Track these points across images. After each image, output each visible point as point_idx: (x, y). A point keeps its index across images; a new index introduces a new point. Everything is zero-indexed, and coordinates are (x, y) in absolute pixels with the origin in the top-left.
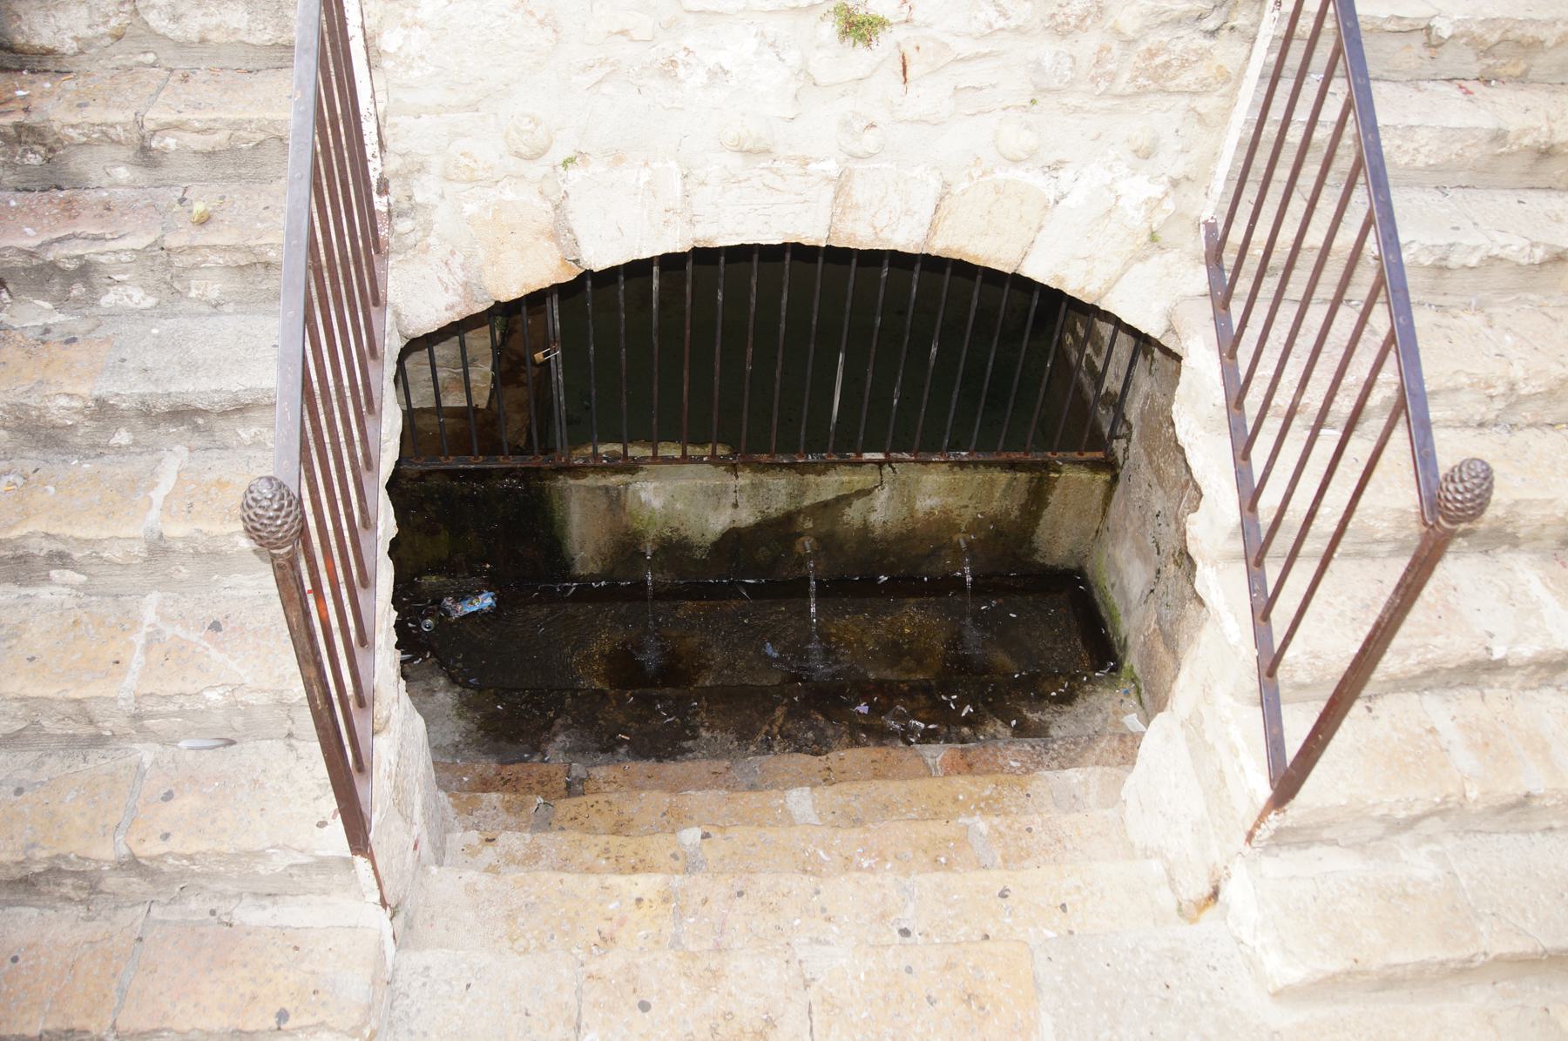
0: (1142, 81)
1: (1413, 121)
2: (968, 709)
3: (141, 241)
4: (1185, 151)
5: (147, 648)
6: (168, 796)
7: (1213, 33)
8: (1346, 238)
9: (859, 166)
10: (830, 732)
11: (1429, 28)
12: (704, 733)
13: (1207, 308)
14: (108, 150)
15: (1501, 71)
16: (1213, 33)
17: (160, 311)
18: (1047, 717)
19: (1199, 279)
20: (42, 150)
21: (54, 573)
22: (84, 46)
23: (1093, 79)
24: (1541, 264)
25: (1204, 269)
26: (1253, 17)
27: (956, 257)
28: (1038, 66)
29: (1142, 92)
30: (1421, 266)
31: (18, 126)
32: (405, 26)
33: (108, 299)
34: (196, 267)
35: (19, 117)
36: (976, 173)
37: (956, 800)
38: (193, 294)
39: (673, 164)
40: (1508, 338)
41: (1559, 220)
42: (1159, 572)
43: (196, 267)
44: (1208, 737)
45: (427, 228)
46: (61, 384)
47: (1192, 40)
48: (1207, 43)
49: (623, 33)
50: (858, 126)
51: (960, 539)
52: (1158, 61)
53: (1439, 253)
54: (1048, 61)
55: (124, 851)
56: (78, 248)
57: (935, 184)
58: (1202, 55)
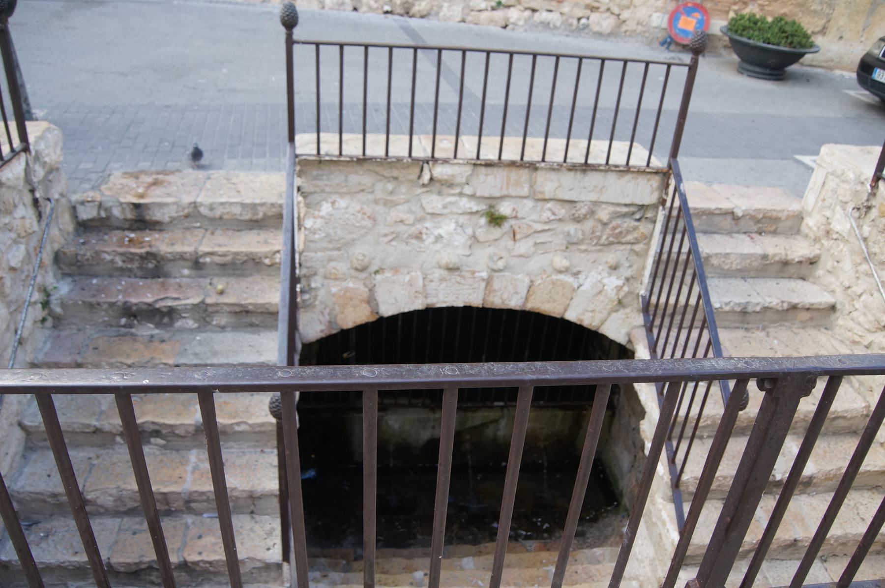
0: (611, 239)
1: (728, 251)
2: (546, 525)
3: (196, 300)
4: (630, 266)
5: (193, 472)
6: (200, 537)
7: (639, 220)
8: (693, 301)
9: (496, 274)
10: (480, 536)
11: (733, 213)
12: (419, 537)
13: (643, 332)
14: (182, 263)
15: (765, 229)
16: (639, 220)
17: (199, 330)
18: (585, 529)
19: (640, 319)
20: (154, 262)
21: (153, 440)
22: (173, 219)
23: (591, 239)
24: (788, 310)
25: (641, 315)
26: (654, 214)
27: (537, 311)
28: (569, 234)
29: (611, 244)
30: (736, 312)
31: (148, 253)
32: (314, 218)
33: (179, 324)
34: (217, 312)
35: (147, 249)
36: (544, 277)
37: (541, 562)
38: (214, 323)
39: (419, 273)
40: (775, 342)
41: (793, 291)
42: (635, 456)
43: (217, 312)
44: (654, 519)
45: (315, 297)
46: (160, 359)
47: (629, 223)
48: (637, 224)
49: (401, 221)
50: (495, 258)
51: (541, 444)
52: (617, 231)
53: (743, 306)
54: (572, 232)
55: (182, 559)
56: (170, 303)
57: (527, 281)
58: (635, 228)
